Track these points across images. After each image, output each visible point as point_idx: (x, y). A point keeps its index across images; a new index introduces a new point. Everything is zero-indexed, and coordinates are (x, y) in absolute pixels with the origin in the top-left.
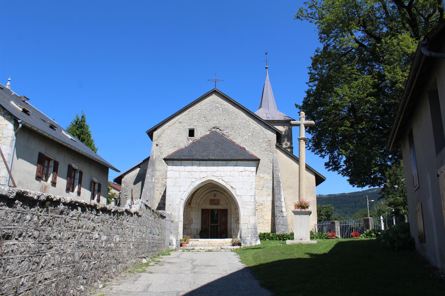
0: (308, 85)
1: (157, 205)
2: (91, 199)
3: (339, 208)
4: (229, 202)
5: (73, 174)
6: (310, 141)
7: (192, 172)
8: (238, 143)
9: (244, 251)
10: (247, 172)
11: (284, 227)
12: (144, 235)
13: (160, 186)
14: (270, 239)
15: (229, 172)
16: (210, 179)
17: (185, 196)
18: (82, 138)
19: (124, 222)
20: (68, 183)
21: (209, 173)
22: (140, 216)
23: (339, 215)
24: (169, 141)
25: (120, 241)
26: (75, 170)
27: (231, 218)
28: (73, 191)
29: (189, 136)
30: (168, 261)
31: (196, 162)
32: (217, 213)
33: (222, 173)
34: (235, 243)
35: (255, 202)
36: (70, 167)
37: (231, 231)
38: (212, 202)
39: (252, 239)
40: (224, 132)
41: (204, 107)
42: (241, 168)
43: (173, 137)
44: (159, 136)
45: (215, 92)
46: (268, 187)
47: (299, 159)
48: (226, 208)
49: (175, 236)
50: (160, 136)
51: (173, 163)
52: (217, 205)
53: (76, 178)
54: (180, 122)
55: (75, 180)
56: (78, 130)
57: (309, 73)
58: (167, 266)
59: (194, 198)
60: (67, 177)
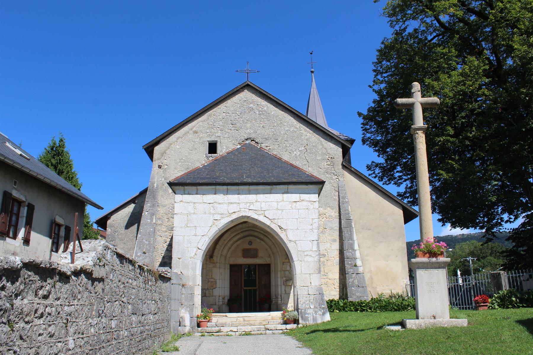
1: (160, 260)
2: (52, 250)
4: (273, 253)
5: (15, 209)
7: (215, 205)
10: (304, 203)
11: (360, 289)
12: (113, 324)
14: (340, 310)
15: (276, 204)
16: (244, 214)
17: (204, 243)
18: (59, 170)
21: (242, 206)
22: (101, 280)
24: (178, 160)
26: (20, 203)
27: (276, 278)
28: (15, 237)
33: (263, 205)
34: (288, 319)
37: (277, 297)
38: (247, 253)
39: (316, 312)
42: (295, 197)
43: (183, 152)
44: (163, 154)
45: (247, 86)
46: (332, 229)
48: (268, 262)
50: (165, 152)
53: (21, 215)
54: (196, 132)
55: (20, 219)
56: (54, 158)
59: (218, 246)
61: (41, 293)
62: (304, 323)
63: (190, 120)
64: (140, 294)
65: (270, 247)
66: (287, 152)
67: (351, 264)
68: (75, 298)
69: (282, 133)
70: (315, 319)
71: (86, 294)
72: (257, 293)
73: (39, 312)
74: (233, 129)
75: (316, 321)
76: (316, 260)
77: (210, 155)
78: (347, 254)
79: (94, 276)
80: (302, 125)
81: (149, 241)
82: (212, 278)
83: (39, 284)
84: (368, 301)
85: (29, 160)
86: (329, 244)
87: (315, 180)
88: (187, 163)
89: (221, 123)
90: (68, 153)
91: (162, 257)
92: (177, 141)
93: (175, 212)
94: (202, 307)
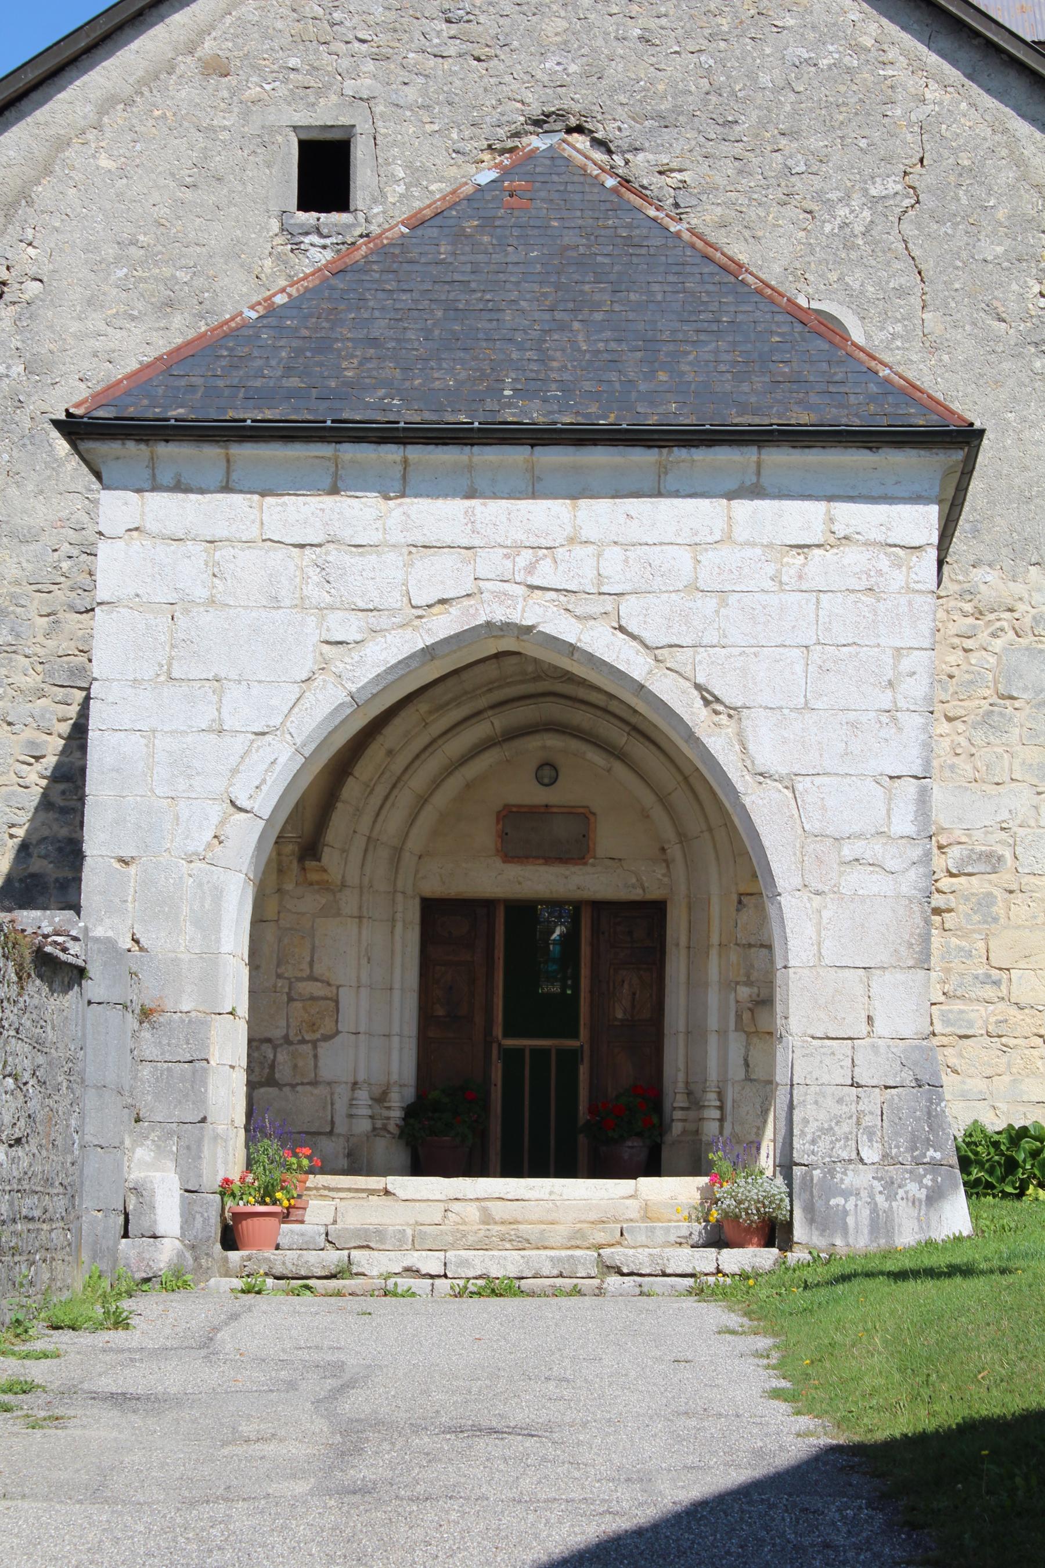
4: (683, 837)
7: (333, 554)
8: (773, 273)
9: (822, 1294)
10: (853, 557)
13: (32, 680)
15: (685, 556)
16: (499, 614)
17: (268, 774)
21: (490, 563)
24: (110, 251)
27: (695, 984)
29: (305, 204)
30: (107, 1384)
32: (571, 940)
35: (930, 836)
37: (695, 1103)
38: (524, 832)
39: (890, 1186)
42: (802, 517)
51: (152, 462)
52: (563, 859)
58: (98, 1430)
59: (351, 790)
62: (819, 1241)
65: (663, 800)
66: (790, 212)
69: (765, 79)
70: (881, 1223)
72: (583, 1071)
75: (889, 1233)
76: (904, 889)
77: (303, 217)
80: (893, 30)
82: (312, 978)
86: (1027, 795)
87: (920, 421)
88: (167, 271)
91: (12, 844)
92: (98, 127)
93: (101, 595)
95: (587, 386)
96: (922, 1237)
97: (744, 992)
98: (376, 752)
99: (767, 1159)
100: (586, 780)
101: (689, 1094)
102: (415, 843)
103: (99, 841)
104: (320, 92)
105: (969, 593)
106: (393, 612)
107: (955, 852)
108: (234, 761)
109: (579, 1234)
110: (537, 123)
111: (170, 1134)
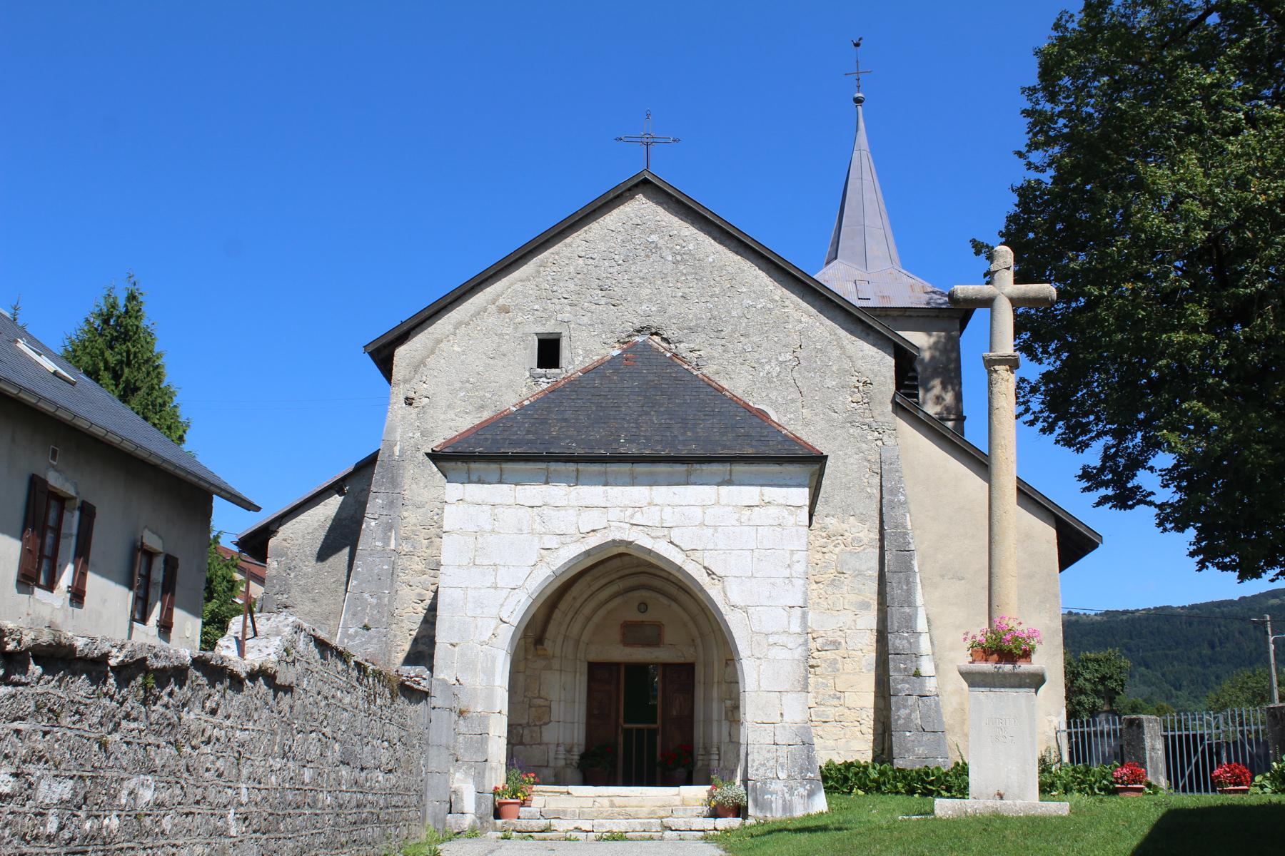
0: (1024, 162)
1: (407, 647)
2: (133, 619)
3: (1147, 667)
4: (701, 635)
5: (52, 515)
6: (1034, 390)
7: (546, 510)
8: (739, 393)
9: (757, 841)
10: (772, 510)
11: (926, 737)
12: (307, 775)
13: (421, 567)
14: (867, 791)
18: (127, 381)
19: (189, 717)
20: (26, 554)
21: (614, 514)
22: (288, 689)
23: (1146, 690)
24: (458, 385)
25: (160, 805)
26: (62, 501)
27: (708, 700)
28: (50, 586)
31: (561, 467)
36: (36, 486)
37: (707, 752)
38: (633, 633)
39: (791, 789)
40: (682, 348)
41: (602, 246)
42: (750, 494)
43: (471, 367)
45: (644, 185)
46: (859, 574)
47: (988, 457)
48: (689, 660)
49: (472, 771)
50: (423, 363)
53: (64, 530)
54: (504, 310)
55: (63, 542)
56: (112, 348)
57: (1026, 113)
59: (557, 615)
60: (24, 530)
61: (208, 704)
62: (760, 815)
63: (491, 277)
64: (358, 724)
66: (745, 367)
67: (905, 669)
68: (249, 717)
69: (734, 313)
70: (787, 807)
71: (265, 713)
72: (659, 739)
73: (207, 735)
74: (603, 301)
75: (791, 811)
78: (895, 642)
79: (278, 681)
81: (380, 598)
82: (540, 697)
83: (207, 690)
84: (945, 770)
85: (73, 384)
86: (851, 615)
87: (800, 452)
88: (481, 393)
89: (572, 287)
90: (150, 335)
92: (454, 334)
94: (507, 769)
95: (657, 438)
96: (805, 813)
97: (729, 703)
98: (568, 598)
99: (738, 781)
100: (659, 611)
101: (705, 748)
102: (585, 638)
103: (443, 635)
104: (547, 319)
105: (824, 528)
106: (572, 536)
107: (820, 640)
108: (501, 601)
109: (653, 812)
110: (638, 331)
111: (471, 767)
